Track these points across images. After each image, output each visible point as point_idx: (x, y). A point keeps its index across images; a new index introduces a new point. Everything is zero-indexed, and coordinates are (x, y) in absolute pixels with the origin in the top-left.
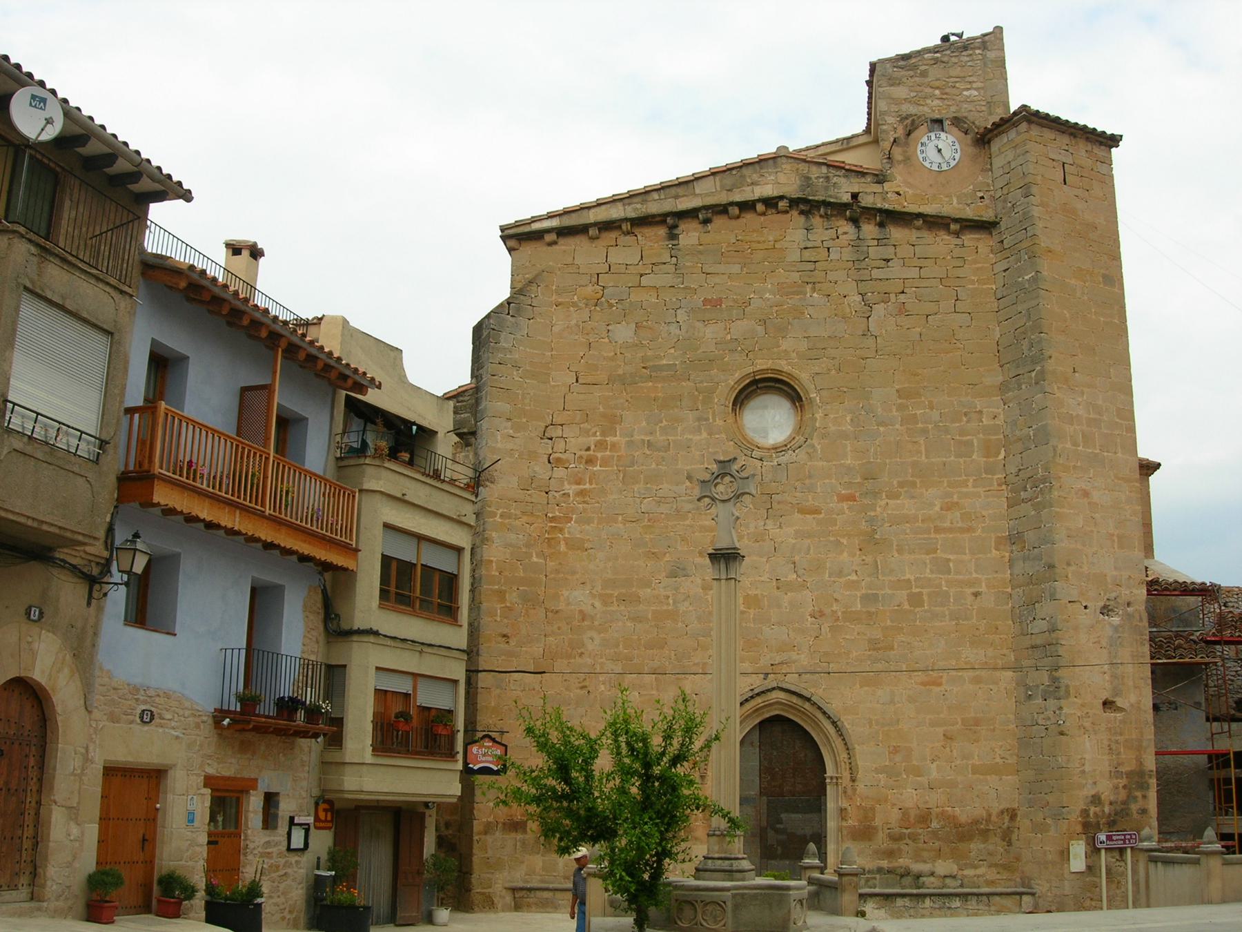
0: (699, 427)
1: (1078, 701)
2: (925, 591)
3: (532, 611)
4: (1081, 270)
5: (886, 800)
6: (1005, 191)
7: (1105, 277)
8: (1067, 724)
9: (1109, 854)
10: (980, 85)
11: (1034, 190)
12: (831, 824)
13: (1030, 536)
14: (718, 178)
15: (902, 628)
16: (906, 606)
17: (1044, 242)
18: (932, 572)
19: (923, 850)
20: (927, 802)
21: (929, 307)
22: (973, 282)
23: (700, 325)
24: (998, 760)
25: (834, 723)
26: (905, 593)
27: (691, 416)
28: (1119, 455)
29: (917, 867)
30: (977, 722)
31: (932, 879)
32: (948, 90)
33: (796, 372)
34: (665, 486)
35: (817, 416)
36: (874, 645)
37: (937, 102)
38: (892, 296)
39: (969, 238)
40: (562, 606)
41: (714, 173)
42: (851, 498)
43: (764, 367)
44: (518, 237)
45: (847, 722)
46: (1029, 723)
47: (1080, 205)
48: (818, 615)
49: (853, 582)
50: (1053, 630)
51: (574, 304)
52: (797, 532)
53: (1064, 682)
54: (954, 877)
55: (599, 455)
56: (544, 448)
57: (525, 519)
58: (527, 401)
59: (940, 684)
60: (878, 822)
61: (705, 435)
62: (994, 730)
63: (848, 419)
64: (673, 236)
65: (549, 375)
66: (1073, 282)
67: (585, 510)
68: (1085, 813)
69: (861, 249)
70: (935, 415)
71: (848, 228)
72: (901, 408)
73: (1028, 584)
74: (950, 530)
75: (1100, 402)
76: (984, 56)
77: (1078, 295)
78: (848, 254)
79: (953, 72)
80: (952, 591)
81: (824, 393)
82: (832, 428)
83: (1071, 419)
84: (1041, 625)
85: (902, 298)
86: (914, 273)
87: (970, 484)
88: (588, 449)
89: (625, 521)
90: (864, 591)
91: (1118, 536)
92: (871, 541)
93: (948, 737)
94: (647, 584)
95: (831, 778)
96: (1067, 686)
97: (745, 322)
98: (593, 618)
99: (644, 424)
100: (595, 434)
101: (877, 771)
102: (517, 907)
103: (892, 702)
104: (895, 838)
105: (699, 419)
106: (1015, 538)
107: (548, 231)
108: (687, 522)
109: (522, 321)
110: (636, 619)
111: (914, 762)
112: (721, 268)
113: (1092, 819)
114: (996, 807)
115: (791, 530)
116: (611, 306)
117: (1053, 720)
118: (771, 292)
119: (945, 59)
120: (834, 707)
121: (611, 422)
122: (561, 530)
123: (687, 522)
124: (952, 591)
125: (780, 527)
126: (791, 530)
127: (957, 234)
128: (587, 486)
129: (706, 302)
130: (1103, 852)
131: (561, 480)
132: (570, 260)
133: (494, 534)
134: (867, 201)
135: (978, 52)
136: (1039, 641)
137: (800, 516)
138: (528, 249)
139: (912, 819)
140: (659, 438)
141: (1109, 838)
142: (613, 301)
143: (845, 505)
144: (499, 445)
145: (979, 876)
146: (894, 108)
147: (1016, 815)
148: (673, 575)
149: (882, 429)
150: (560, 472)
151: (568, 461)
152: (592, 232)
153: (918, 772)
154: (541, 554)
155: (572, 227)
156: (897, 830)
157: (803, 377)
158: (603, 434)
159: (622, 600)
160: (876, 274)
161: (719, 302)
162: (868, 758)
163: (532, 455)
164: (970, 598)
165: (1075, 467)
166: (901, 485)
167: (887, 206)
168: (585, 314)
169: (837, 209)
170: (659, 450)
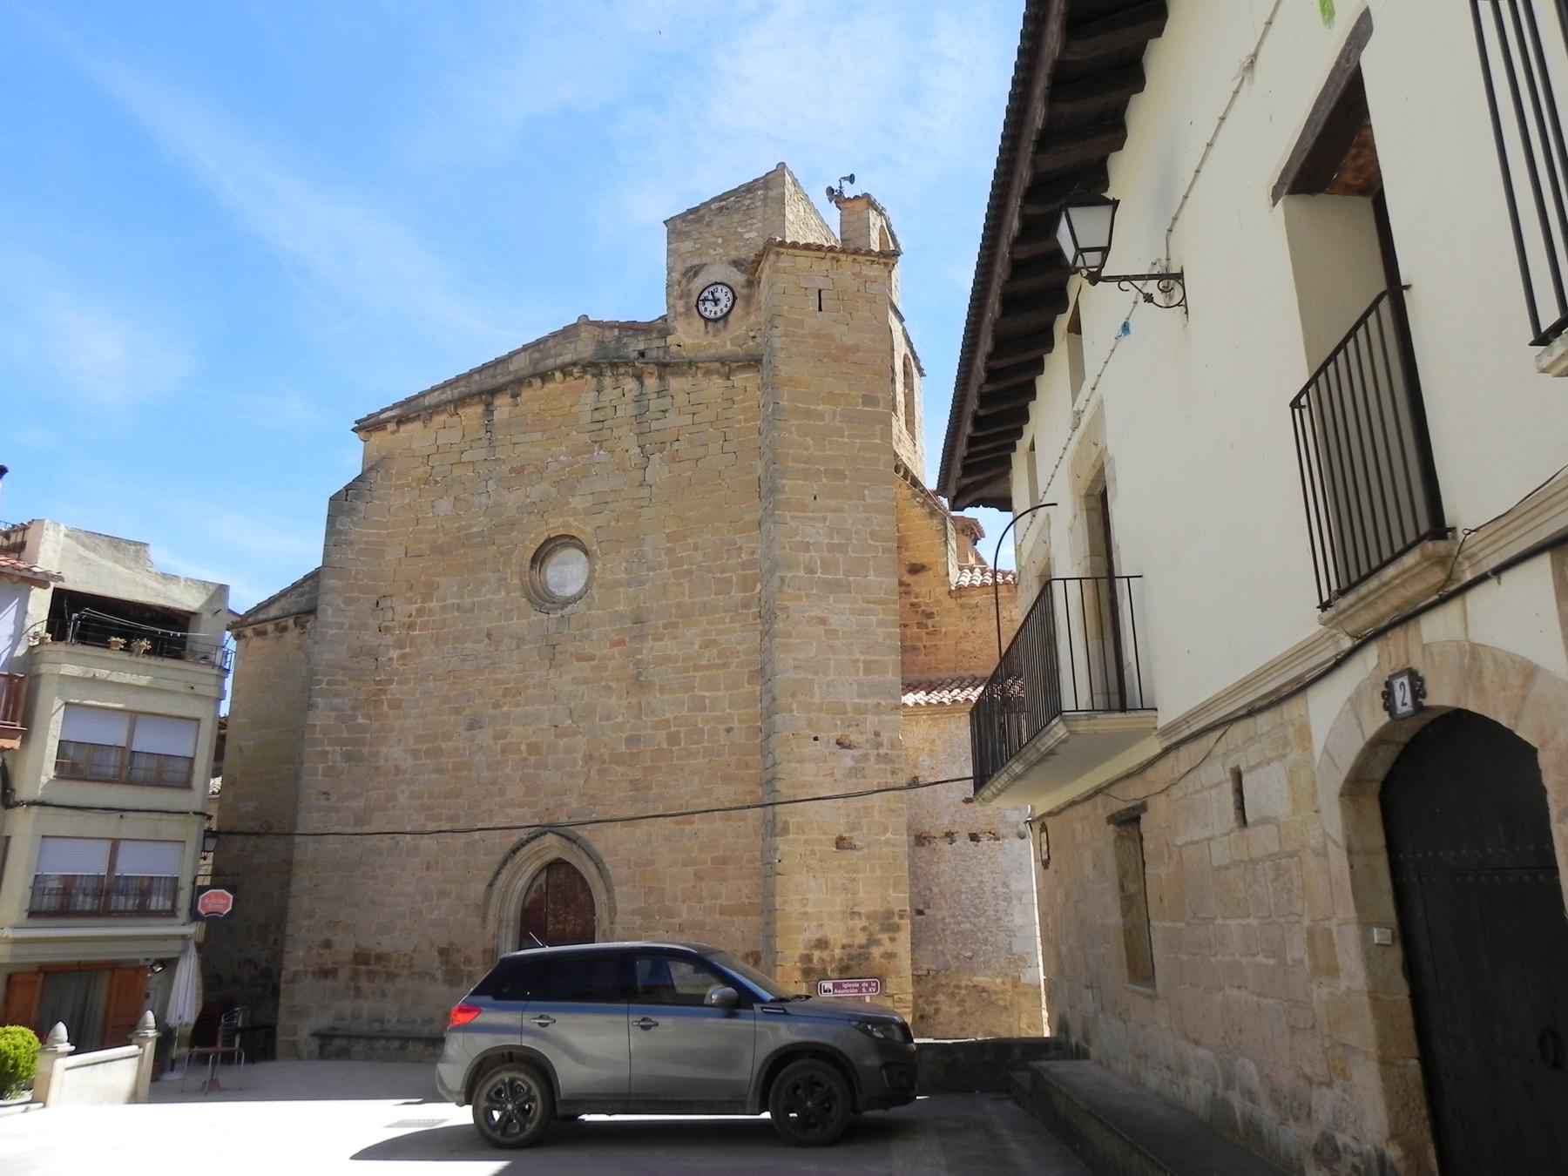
1: (802, 837)
11: (778, 321)
23: (505, 492)
24: (744, 899)
26: (664, 732)
28: (872, 578)
30: (725, 861)
34: (469, 645)
36: (635, 785)
41: (525, 348)
42: (621, 643)
44: (367, 427)
48: (590, 758)
61: (503, 593)
64: (489, 411)
68: (807, 958)
70: (699, 556)
72: (670, 551)
74: (707, 667)
80: (707, 728)
83: (806, 547)
92: (639, 683)
93: (698, 877)
96: (786, 823)
101: (636, 912)
102: (323, 1055)
107: (388, 421)
110: (439, 770)
112: (526, 437)
118: (566, 455)
121: (430, 589)
122: (385, 692)
124: (707, 728)
138: (377, 437)
143: (616, 650)
148: (470, 728)
153: (670, 913)
154: (368, 716)
155: (411, 411)
158: (423, 601)
159: (428, 754)
160: (654, 425)
161: (523, 468)
163: (364, 626)
164: (722, 734)
166: (665, 627)
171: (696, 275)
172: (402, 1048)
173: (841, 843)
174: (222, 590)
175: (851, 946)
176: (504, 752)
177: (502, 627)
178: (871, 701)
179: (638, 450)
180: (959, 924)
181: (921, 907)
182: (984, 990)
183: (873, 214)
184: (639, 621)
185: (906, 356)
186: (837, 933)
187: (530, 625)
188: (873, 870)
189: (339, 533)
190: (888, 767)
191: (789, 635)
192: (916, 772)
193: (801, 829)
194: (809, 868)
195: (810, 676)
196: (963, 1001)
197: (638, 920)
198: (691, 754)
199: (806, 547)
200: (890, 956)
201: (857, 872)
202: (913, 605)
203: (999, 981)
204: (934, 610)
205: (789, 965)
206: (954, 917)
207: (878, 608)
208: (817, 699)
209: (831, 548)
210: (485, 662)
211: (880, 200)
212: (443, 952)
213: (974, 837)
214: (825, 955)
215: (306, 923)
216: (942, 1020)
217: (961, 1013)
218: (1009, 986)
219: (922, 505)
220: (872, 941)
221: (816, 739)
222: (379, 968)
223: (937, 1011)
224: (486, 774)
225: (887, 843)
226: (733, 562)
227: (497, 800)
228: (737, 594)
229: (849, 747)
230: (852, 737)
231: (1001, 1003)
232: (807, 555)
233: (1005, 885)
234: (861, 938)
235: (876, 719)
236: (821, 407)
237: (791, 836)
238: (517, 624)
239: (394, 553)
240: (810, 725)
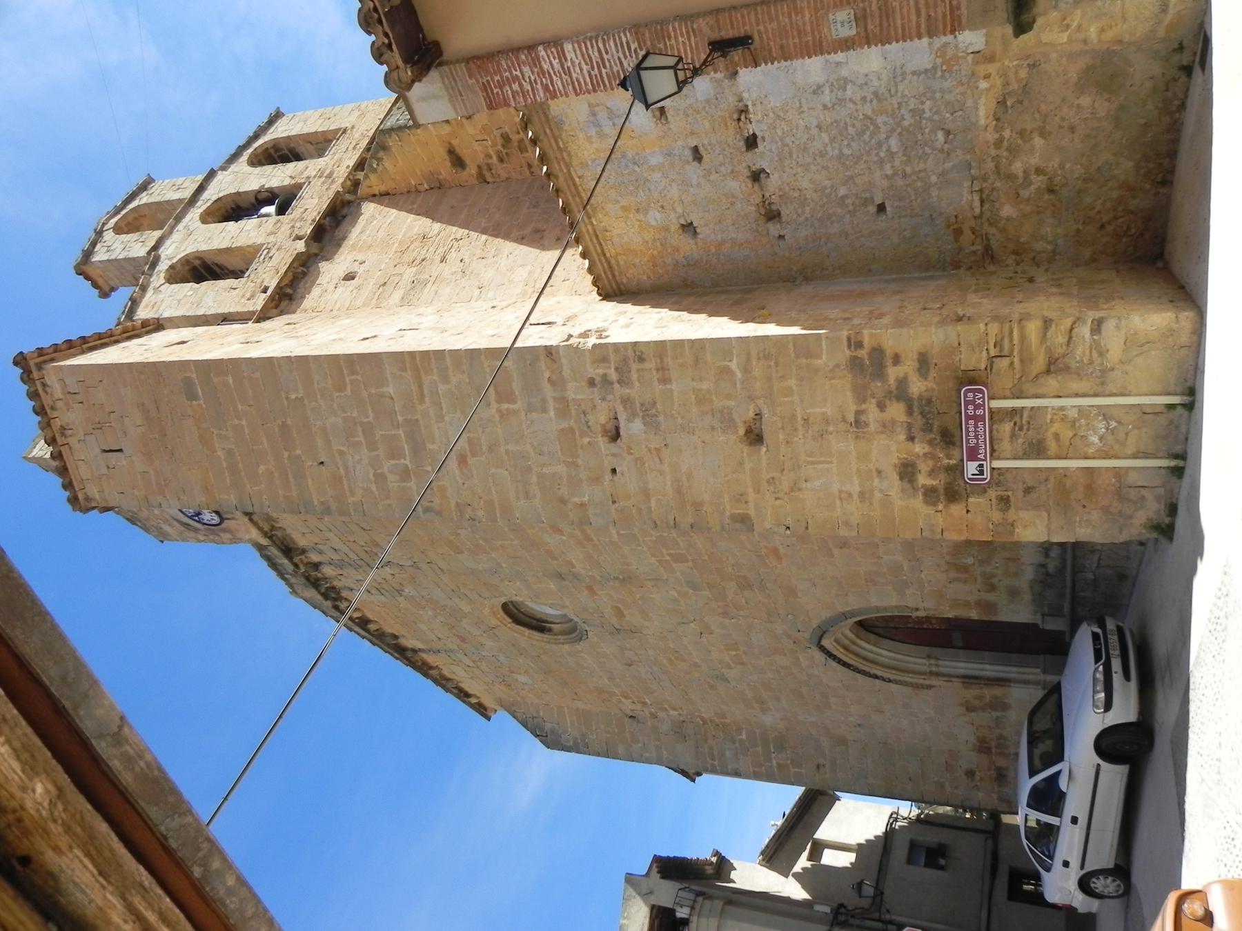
1: (751, 496)
68: (930, 495)
83: (380, 477)
154: (739, 731)
173: (755, 437)
174: (630, 879)
175: (909, 427)
178: (548, 391)
180: (891, 155)
181: (872, 209)
182: (1002, 103)
183: (100, 255)
185: (256, 161)
186: (889, 449)
188: (788, 392)
189: (575, 743)
190: (635, 367)
191: (490, 503)
192: (674, 227)
193: (740, 498)
194: (795, 487)
195: (534, 479)
196: (1022, 133)
199: (380, 477)
200: (923, 362)
201: (794, 416)
202: (501, 160)
203: (983, 85)
204: (497, 133)
205: (940, 521)
206: (881, 162)
207: (426, 380)
208: (561, 469)
211: (77, 255)
213: (752, 142)
214: (924, 467)
215: (948, 789)
216: (1055, 163)
217: (1043, 134)
218: (992, 68)
219: (379, 160)
220: (901, 392)
221: (614, 471)
223: (1039, 171)
225: (746, 370)
229: (617, 429)
230: (603, 420)
231: (1023, 73)
233: (818, 90)
234: (896, 411)
235: (571, 385)
236: (220, 453)
237: (752, 512)
240: (597, 480)
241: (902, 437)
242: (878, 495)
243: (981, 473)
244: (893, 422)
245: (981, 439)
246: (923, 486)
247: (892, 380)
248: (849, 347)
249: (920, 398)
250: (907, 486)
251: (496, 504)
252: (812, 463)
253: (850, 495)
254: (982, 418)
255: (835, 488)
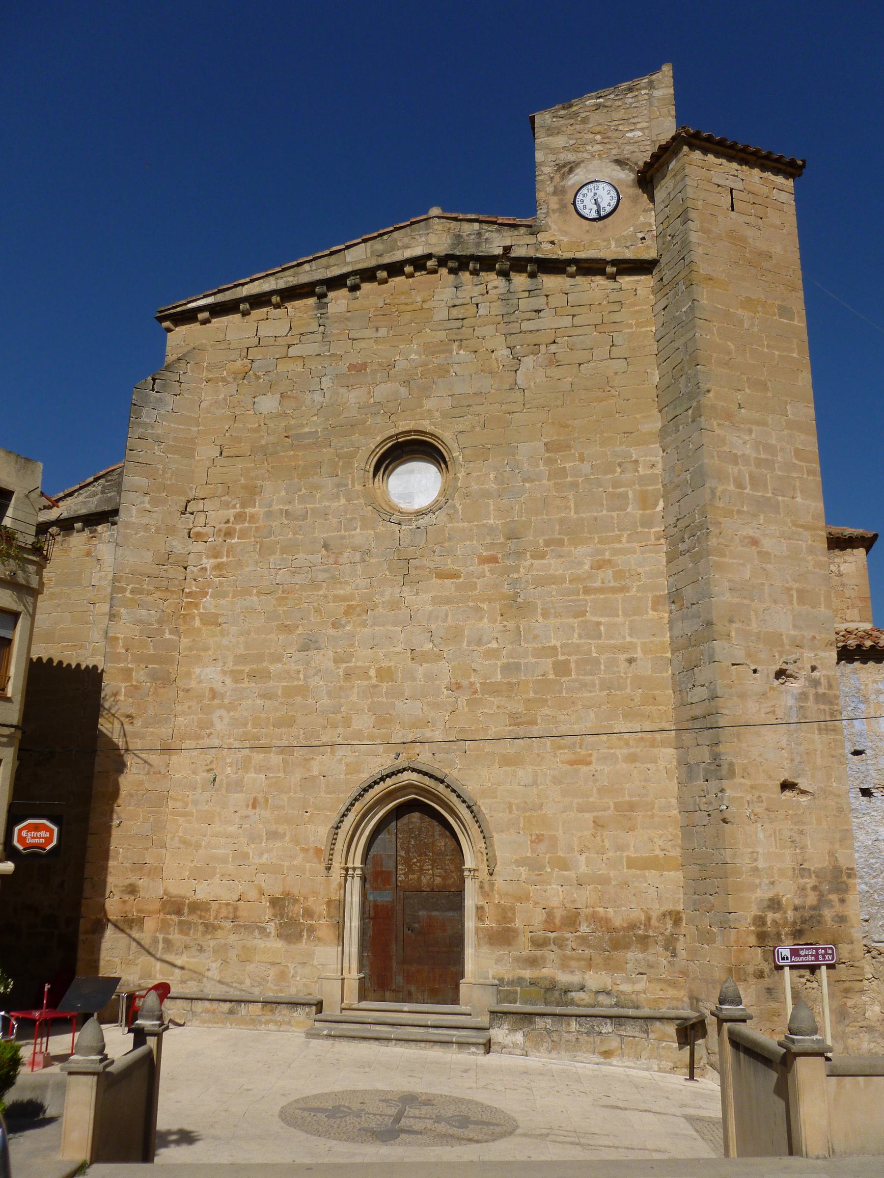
0: (338, 493)
2: (572, 658)
3: (162, 690)
4: (750, 299)
5: (528, 898)
6: (665, 225)
7: (780, 308)
8: (732, 809)
9: (796, 972)
10: (645, 125)
11: (693, 214)
12: (470, 924)
13: (689, 592)
14: (369, 244)
15: (547, 701)
16: (551, 676)
17: (703, 268)
18: (580, 637)
19: (571, 958)
20: (574, 901)
21: (579, 356)
22: (630, 326)
23: (343, 390)
25: (365, 790)
27: (329, 482)
28: (799, 499)
29: (564, 978)
30: (632, 807)
31: (582, 995)
32: (610, 134)
33: (438, 432)
34: (301, 556)
35: (459, 475)
36: (515, 719)
37: (598, 147)
38: (543, 348)
39: (626, 281)
40: (193, 684)
42: (493, 560)
43: (407, 429)
45: (484, 806)
46: (691, 808)
47: (750, 233)
48: (455, 687)
49: (494, 650)
50: (714, 697)
51: (224, 380)
52: (433, 598)
53: (726, 759)
54: (608, 993)
55: (238, 527)
56: (183, 523)
57: (158, 594)
58: (168, 475)
59: (589, 763)
60: (518, 924)
61: (343, 501)
62: (653, 816)
63: (492, 476)
64: (322, 306)
65: (194, 450)
66: (740, 312)
67: (221, 583)
68: (760, 921)
69: (510, 302)
70: (586, 467)
71: (500, 282)
72: (549, 462)
73: (687, 648)
74: (601, 590)
75: (774, 442)
76: (650, 96)
77: (746, 326)
78: (497, 308)
79: (615, 116)
81: (467, 451)
82: (475, 487)
83: (734, 459)
84: (700, 693)
85: (553, 348)
86: (567, 321)
87: (624, 540)
88: (228, 522)
89: (259, 593)
90: (505, 660)
91: (798, 591)
92: (515, 606)
93: (598, 824)
94: (278, 659)
95: (470, 871)
96: (731, 764)
97: (389, 385)
98: (223, 696)
99: (283, 493)
100: (234, 507)
101: (520, 863)
103: (535, 783)
104: (539, 943)
105: (338, 486)
106: (675, 597)
107: (201, 309)
108: (321, 592)
109: (168, 398)
110: (266, 696)
111: (560, 854)
113: (769, 928)
114: (657, 910)
115: (427, 597)
116: (258, 377)
117: (715, 805)
119: (608, 104)
120: (471, 788)
121: (252, 493)
122: (196, 605)
123: (321, 592)
125: (417, 594)
126: (427, 597)
127: (613, 277)
128: (224, 559)
129: (351, 367)
130: (787, 969)
131: (199, 554)
132: (221, 336)
133: (122, 610)
134: (519, 252)
135: (643, 92)
136: (698, 711)
137: (439, 581)
139: (557, 921)
140: (298, 507)
141: (795, 953)
142: (260, 374)
143: (486, 567)
144: (134, 520)
145: (638, 993)
146: (551, 157)
147: (680, 919)
148: (305, 648)
149: (527, 485)
150: (200, 547)
151: (207, 534)
152: (243, 307)
153: (564, 865)
154: (176, 631)
156: (541, 933)
157: (447, 437)
158: (243, 506)
159: (253, 676)
160: (526, 326)
161: (364, 366)
162: (505, 847)
163: (171, 530)
165: (739, 512)
166: (548, 543)
167: (539, 255)
168: (234, 387)
169: (487, 263)
170: (296, 519)
171: (571, 170)
172: (231, 1012)
175: (804, 908)
176: (348, 675)
177: (343, 538)
178: (808, 634)
179: (507, 352)
184: (512, 536)
187: (377, 537)
190: (827, 708)
197: (524, 871)
198: (584, 686)
199: (734, 459)
201: (803, 823)
209: (759, 463)
210: (322, 576)
212: (275, 902)
214: (777, 916)
222: (193, 918)
224: (325, 701)
226: (628, 476)
227: (340, 730)
228: (633, 510)
232: (736, 470)
234: (812, 899)
238: (359, 535)
239: (206, 452)
241: (797, 902)
242: (757, 881)
243: (783, 959)
244: (806, 896)
245: (804, 959)
246: (766, 915)
247: (831, 897)
248: (848, 869)
249: (820, 916)
250: (766, 903)
251: (722, 559)
252: (775, 832)
253: (756, 860)
254: (817, 960)
255: (760, 850)
